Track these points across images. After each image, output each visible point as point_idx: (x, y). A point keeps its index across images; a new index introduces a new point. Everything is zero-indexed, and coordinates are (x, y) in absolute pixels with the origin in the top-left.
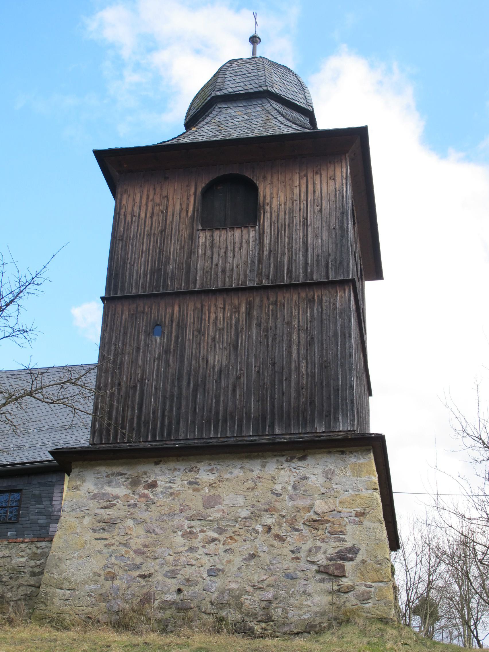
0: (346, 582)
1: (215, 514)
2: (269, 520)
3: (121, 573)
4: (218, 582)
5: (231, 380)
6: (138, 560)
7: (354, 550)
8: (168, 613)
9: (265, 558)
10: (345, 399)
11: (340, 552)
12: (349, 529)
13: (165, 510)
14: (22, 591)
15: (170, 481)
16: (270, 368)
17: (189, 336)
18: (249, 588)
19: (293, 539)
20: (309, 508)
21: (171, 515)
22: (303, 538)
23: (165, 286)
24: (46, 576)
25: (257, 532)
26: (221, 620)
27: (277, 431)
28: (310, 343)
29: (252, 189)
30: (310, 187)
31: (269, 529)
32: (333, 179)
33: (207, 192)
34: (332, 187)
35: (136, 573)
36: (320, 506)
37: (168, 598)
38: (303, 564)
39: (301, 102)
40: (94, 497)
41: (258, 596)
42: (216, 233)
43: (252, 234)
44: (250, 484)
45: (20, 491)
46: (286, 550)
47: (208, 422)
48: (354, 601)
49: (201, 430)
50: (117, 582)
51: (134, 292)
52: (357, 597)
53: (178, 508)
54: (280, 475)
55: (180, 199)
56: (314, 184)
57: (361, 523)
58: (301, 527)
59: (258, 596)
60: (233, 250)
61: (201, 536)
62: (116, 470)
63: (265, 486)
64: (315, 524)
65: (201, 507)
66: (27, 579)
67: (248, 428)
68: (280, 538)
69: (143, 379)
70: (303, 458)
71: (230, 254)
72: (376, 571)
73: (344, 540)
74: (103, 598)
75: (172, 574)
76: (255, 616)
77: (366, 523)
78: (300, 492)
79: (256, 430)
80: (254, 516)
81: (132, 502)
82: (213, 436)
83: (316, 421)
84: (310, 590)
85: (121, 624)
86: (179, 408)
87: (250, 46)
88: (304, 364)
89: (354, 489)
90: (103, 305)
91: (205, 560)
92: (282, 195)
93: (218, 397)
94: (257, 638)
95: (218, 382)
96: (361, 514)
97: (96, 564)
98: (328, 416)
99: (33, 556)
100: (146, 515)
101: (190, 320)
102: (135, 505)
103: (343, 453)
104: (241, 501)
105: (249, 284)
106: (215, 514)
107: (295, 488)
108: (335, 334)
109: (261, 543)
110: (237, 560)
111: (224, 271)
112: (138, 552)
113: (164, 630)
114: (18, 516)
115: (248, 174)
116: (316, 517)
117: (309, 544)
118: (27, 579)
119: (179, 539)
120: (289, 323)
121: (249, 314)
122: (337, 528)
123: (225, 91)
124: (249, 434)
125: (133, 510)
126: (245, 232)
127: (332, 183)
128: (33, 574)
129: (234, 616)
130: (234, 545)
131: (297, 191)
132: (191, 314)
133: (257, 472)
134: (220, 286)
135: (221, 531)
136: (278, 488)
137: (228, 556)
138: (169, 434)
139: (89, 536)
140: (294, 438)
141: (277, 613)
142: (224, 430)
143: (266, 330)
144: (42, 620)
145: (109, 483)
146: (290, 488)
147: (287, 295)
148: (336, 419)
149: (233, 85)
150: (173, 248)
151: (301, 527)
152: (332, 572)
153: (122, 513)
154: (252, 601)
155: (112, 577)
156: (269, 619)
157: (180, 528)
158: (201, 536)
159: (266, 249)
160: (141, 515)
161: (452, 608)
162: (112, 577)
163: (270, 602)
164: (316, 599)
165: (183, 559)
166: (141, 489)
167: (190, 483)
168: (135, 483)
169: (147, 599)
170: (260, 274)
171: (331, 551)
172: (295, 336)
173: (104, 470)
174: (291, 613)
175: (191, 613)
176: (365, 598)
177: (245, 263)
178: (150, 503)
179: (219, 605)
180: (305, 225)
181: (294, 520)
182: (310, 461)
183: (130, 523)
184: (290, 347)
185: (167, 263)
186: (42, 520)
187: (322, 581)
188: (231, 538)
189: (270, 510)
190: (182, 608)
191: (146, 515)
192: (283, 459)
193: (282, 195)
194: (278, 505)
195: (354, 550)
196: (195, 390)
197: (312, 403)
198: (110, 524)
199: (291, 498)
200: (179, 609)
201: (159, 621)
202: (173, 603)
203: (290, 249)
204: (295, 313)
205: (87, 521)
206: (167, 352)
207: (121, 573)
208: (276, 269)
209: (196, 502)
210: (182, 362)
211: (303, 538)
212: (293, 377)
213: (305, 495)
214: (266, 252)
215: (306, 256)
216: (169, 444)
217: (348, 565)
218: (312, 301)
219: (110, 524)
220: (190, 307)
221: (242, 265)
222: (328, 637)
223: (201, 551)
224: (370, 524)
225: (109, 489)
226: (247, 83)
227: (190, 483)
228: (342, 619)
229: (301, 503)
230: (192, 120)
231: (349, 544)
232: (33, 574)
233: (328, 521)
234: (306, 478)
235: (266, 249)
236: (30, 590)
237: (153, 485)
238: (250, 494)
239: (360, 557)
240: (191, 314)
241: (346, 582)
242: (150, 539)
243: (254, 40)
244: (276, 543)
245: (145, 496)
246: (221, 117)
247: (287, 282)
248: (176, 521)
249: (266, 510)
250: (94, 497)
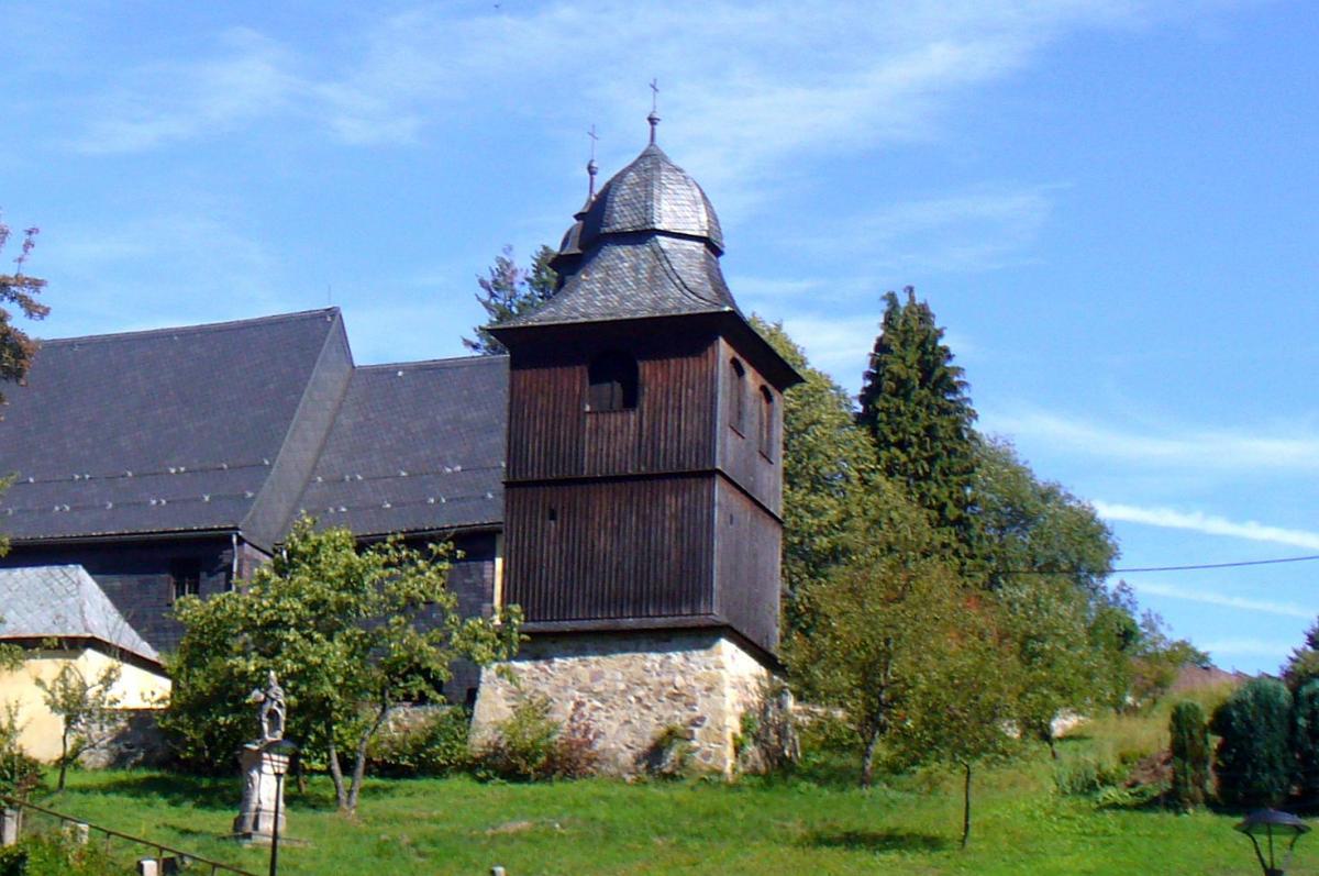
2: (641, 693)
7: (702, 719)
11: (692, 720)
12: (700, 701)
13: (561, 683)
25: (630, 701)
43: (632, 417)
57: (708, 696)
58: (664, 699)
65: (588, 681)
67: (628, 610)
72: (717, 735)
73: (694, 710)
78: (665, 669)
81: (535, 675)
83: (684, 603)
102: (537, 679)
107: (661, 666)
110: (615, 725)
116: (676, 691)
122: (691, 700)
123: (613, 227)
125: (535, 682)
137: (610, 722)
146: (657, 666)
147: (661, 484)
151: (664, 699)
161: (333, 568)
171: (685, 719)
188: (611, 707)
192: (651, 641)
194: (648, 680)
195: (702, 719)
217: (697, 731)
224: (716, 698)
226: (635, 217)
229: (665, 678)
231: (698, 714)
233: (684, 695)
238: (625, 671)
239: (706, 724)
244: (645, 711)
249: (638, 684)
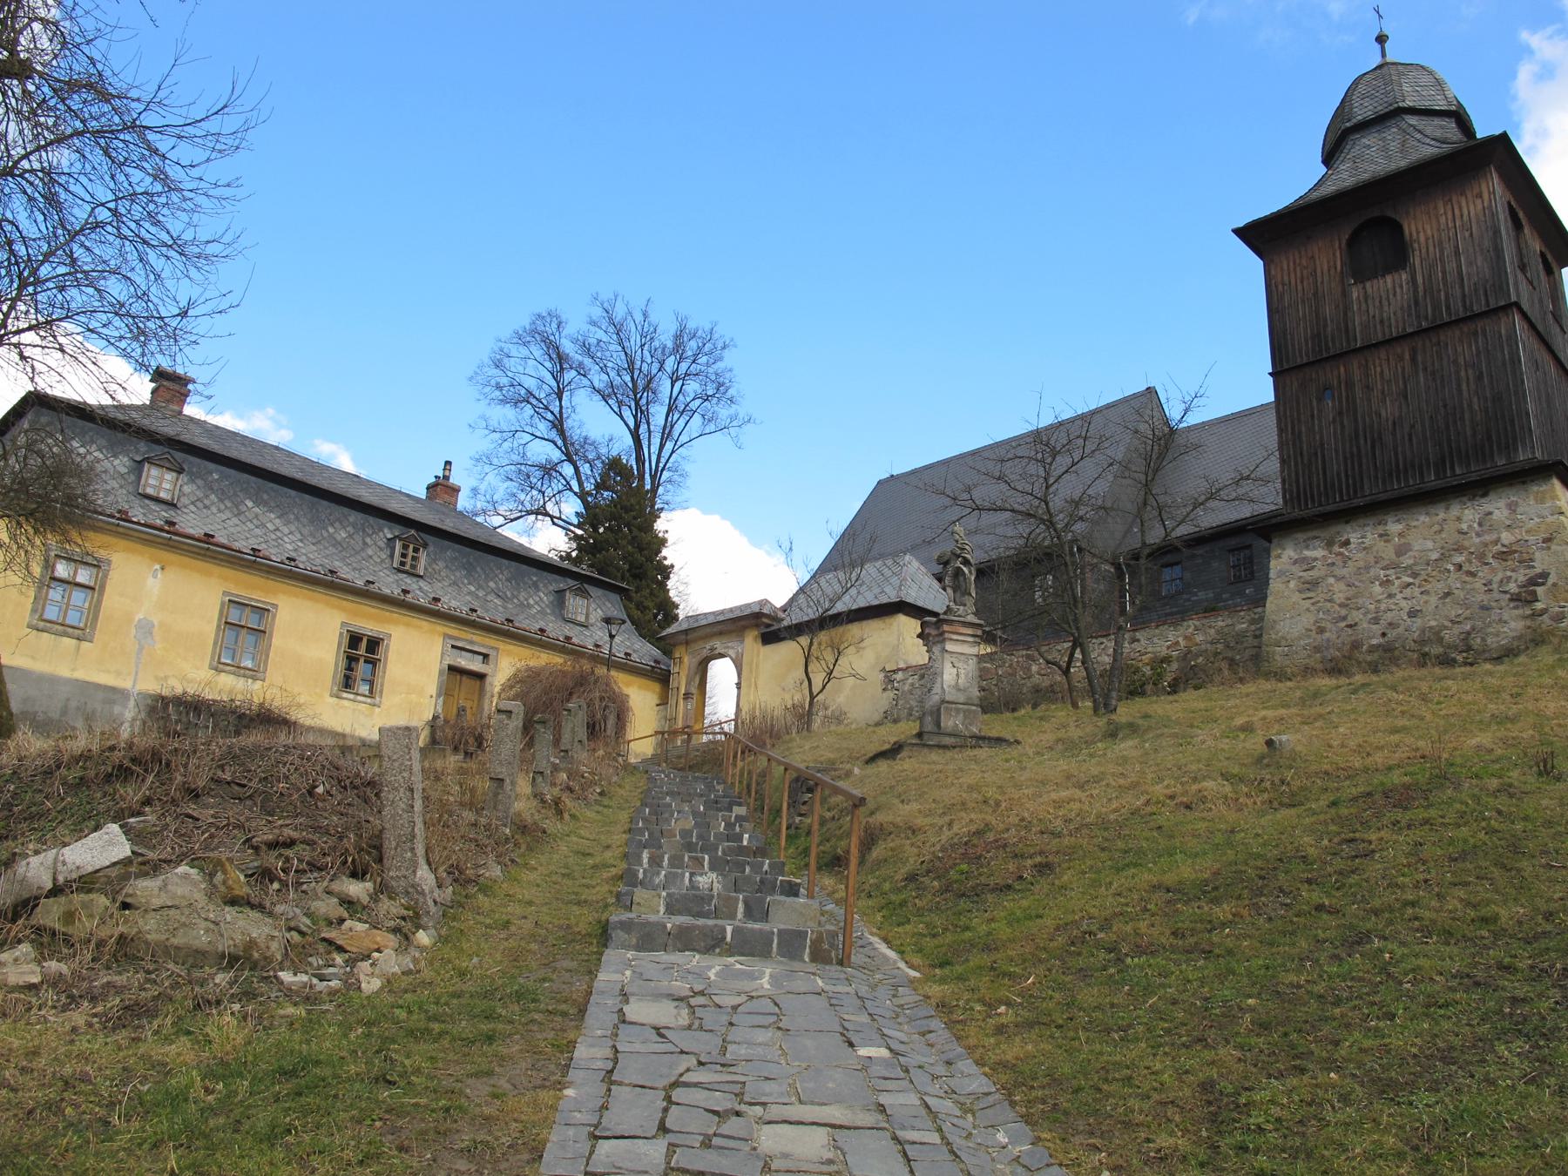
0: (1539, 606)
1: (1407, 561)
2: (1459, 559)
3: (1329, 625)
4: (1419, 622)
5: (1407, 430)
6: (1343, 612)
7: (1544, 575)
8: (1376, 656)
9: (1460, 594)
10: (1522, 428)
13: (1361, 564)
14: (1248, 653)
15: (1362, 538)
16: (1442, 411)
17: (1359, 393)
18: (1447, 623)
19: (1484, 573)
20: (1496, 542)
21: (1367, 568)
22: (1494, 571)
23: (1328, 349)
24: (1265, 637)
26: (1425, 655)
27: (1458, 471)
28: (1480, 378)
29: (1397, 228)
30: (1457, 212)
31: (1459, 567)
33: (1351, 242)
34: (1480, 207)
35: (1343, 624)
36: (1506, 537)
37: (1374, 642)
38: (1496, 595)
39: (1441, 105)
40: (1295, 562)
41: (1457, 630)
42: (1368, 284)
43: (1404, 277)
44: (1436, 527)
45: (1249, 547)
46: (1478, 585)
47: (1391, 475)
48: (1549, 622)
49: (1384, 482)
50: (1327, 635)
51: (1299, 362)
52: (1552, 619)
53: (1372, 560)
54: (1466, 515)
55: (1325, 256)
56: (1461, 209)
59: (1457, 630)
60: (1387, 298)
61: (1397, 583)
62: (1310, 534)
63: (1451, 527)
64: (1502, 556)
66: (1251, 641)
68: (1473, 574)
69: (1322, 445)
70: (1484, 495)
71: (1385, 303)
74: (1317, 649)
75: (1376, 621)
76: (1456, 647)
77: (1554, 547)
79: (1437, 474)
80: (1444, 557)
82: (1397, 487)
84: (1506, 617)
85: (1335, 669)
86: (1360, 465)
87: (1377, 47)
88: (1475, 400)
89: (1539, 516)
91: (1403, 604)
92: (1428, 227)
93: (1395, 448)
94: (1498, 660)
95: (1394, 434)
96: (1548, 540)
97: (1307, 620)
98: (1507, 447)
99: (1253, 622)
100: (1344, 572)
101: (1357, 378)
103: (1524, 483)
104: (1430, 544)
105: (1409, 330)
106: (1407, 561)
107: (1480, 524)
108: (1504, 364)
109: (1454, 581)
110: (1433, 600)
111: (1382, 322)
112: (1340, 605)
113: (1376, 671)
114: (1252, 573)
115: (1390, 213)
117: (1500, 575)
118: (1251, 641)
119: (1377, 588)
120: (1455, 362)
121: (1413, 359)
124: (1432, 480)
126: (1396, 276)
127: (1479, 202)
128: (1256, 637)
129: (1436, 650)
130: (1428, 587)
131: (1443, 220)
132: (1357, 372)
133: (1442, 515)
134: (1380, 338)
135: (1415, 575)
136: (1464, 527)
137: (1425, 597)
138: (1355, 492)
139: (1296, 597)
140: (1474, 477)
141: (1476, 642)
142: (1406, 480)
143: (1433, 373)
144: (1267, 675)
145: (1307, 547)
148: (1516, 450)
149: (1363, 111)
150: (1328, 310)
152: (1525, 598)
153: (1323, 573)
154: (1450, 635)
155: (1321, 630)
156: (1469, 649)
157: (1377, 578)
158: (1397, 583)
159: (1421, 289)
160: (1339, 572)
162: (1321, 630)
163: (1469, 633)
164: (1513, 624)
165: (1383, 606)
166: (1336, 549)
167: (1381, 536)
168: (1330, 544)
169: (1356, 645)
170: (1418, 317)
171: (1522, 579)
172: (1463, 373)
173: (1301, 536)
174: (1489, 641)
175: (1397, 653)
176: (1559, 618)
177: (1402, 308)
178: (1346, 560)
179: (1422, 642)
180: (1457, 253)
181: (1481, 557)
182: (1492, 496)
183: (1331, 580)
184: (1459, 385)
185: (1325, 326)
187: (1516, 608)
189: (1459, 549)
190: (1388, 649)
191: (1344, 572)
193: (1428, 227)
194: (1466, 543)
196: (1373, 447)
197: (1489, 438)
198: (1313, 584)
199: (1478, 535)
200: (1385, 651)
201: (1370, 664)
202: (1379, 645)
203: (1445, 284)
204: (1459, 349)
205: (1292, 584)
206: (1340, 413)
207: (1329, 625)
208: (1434, 310)
209: (1388, 552)
210: (1356, 420)
211: (1494, 571)
212: (1467, 416)
213: (1491, 529)
214: (1421, 294)
215: (1462, 286)
216: (1359, 502)
217: (1540, 590)
218: (1475, 334)
219: (1313, 584)
220: (1355, 364)
221: (1399, 313)
222: (1522, 658)
223: (1399, 596)
225: (1307, 553)
227: (1381, 536)
228: (1537, 640)
229: (1488, 538)
230: (1329, 158)
231: (1538, 570)
232: (1256, 637)
234: (1490, 513)
235: (1421, 289)
236: (1254, 652)
237: (1347, 543)
239: (1550, 581)
240: (1357, 372)
241: (1539, 606)
242: (1351, 592)
243: (1381, 39)
245: (1341, 554)
246: (1355, 151)
247: (1446, 318)
248: (1372, 572)
250: (1295, 562)
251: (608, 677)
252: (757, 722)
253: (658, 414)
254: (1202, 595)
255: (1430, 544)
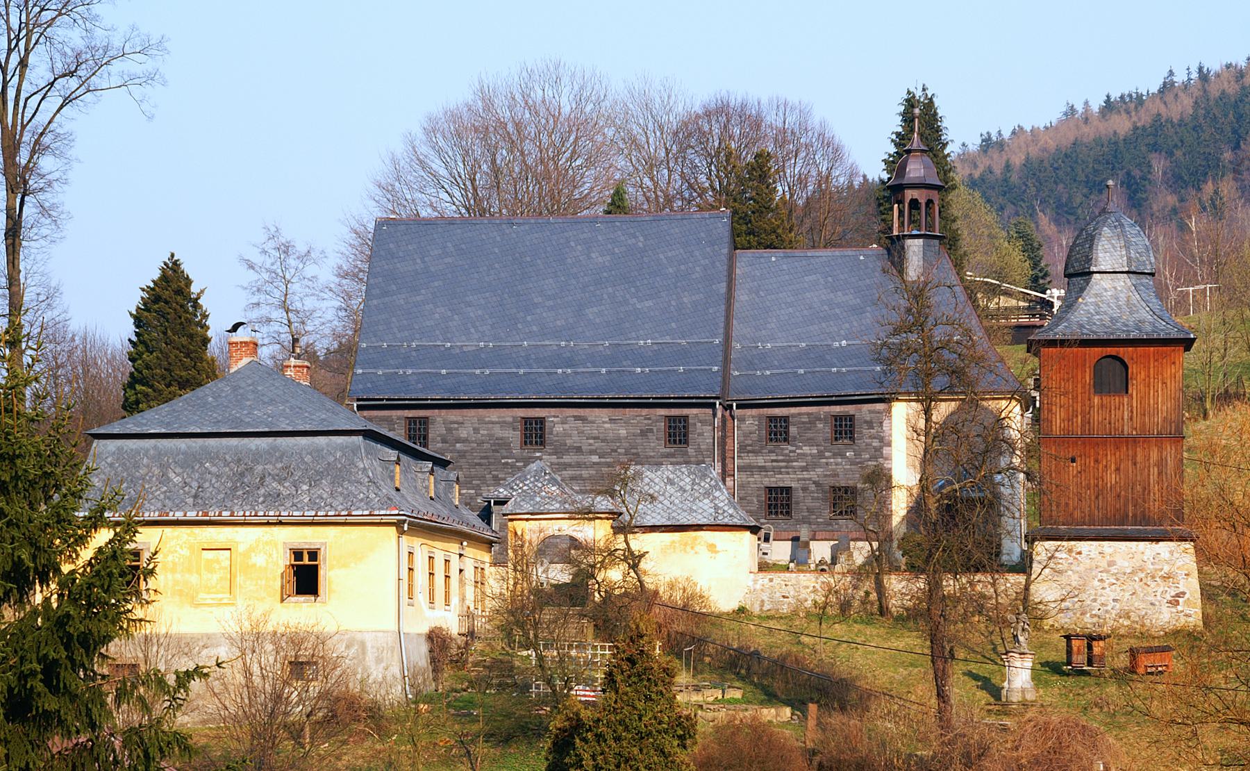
0: (1180, 608)
1: (1113, 570)
2: (1143, 575)
7: (1184, 593)
32: (844, 429)
90: (1041, 123)
110: (1127, 595)
117: (1161, 589)
119: (1096, 583)
171: (1173, 593)
181: (1153, 577)
183: (1070, 573)
186: (876, 443)
189: (1142, 570)
195: (1184, 593)
217: (1181, 600)
239: (1187, 596)
251: (484, 527)
252: (607, 103)
253: (34, 37)
254: (806, 449)
255: (1126, 564)
